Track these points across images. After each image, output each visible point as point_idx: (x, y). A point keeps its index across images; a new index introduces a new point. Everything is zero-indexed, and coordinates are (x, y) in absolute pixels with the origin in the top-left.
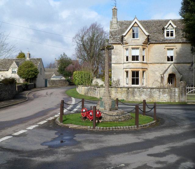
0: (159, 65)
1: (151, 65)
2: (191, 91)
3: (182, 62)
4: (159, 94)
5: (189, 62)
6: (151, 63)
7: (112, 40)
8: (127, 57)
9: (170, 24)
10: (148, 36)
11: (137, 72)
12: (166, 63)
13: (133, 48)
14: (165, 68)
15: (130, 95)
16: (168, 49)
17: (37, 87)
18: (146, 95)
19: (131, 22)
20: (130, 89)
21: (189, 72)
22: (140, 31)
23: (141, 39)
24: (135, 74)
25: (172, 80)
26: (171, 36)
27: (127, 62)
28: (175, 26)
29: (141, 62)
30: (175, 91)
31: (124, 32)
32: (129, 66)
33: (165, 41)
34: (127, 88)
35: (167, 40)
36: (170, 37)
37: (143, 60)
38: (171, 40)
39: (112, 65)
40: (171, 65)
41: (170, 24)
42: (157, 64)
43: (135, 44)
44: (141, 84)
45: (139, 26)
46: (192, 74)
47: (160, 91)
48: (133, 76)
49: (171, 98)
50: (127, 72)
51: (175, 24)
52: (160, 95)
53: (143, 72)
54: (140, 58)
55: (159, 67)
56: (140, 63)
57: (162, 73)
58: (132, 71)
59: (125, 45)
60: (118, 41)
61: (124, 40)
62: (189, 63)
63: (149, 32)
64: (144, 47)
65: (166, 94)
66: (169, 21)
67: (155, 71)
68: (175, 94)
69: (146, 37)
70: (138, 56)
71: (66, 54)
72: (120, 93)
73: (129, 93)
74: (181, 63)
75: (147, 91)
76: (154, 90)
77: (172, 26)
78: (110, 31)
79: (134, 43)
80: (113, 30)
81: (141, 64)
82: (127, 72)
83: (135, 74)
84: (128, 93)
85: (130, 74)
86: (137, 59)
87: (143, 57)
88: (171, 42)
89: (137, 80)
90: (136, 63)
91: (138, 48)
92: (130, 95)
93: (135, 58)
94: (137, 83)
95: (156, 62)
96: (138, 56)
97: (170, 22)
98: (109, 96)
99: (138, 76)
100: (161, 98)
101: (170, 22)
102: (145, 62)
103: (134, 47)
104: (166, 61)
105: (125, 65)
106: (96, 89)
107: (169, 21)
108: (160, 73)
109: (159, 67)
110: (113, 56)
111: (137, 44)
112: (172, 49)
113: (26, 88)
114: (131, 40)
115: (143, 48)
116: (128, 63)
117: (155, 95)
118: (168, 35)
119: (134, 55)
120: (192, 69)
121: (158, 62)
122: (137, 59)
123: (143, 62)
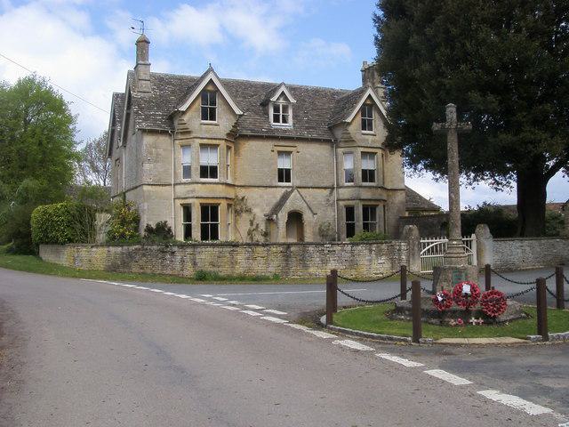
0: (260, 191)
2: (427, 248)
3: (310, 185)
6: (243, 184)
7: (144, 120)
9: (283, 93)
11: (215, 208)
12: (276, 187)
13: (203, 146)
14: (274, 197)
16: (280, 153)
18: (339, 260)
19: (198, 82)
20: (292, 249)
23: (223, 124)
24: (209, 212)
28: (292, 100)
29: (223, 181)
30: (399, 250)
32: (192, 191)
34: (284, 244)
40: (292, 191)
41: (283, 93)
47: (371, 251)
48: (204, 217)
51: (294, 96)
52: (370, 261)
56: (223, 184)
57: (268, 210)
59: (180, 137)
62: (325, 188)
66: (280, 86)
68: (400, 256)
70: (289, 170)
72: (262, 261)
75: (343, 250)
79: (207, 132)
81: (224, 187)
83: (209, 212)
89: (215, 228)
91: (215, 147)
92: (294, 264)
96: (190, 167)
97: (283, 89)
99: (215, 217)
100: (373, 266)
101: (283, 89)
103: (205, 141)
107: (280, 86)
108: (263, 211)
112: (288, 153)
113: (408, 221)
114: (199, 123)
115: (227, 146)
116: (190, 183)
118: (276, 119)
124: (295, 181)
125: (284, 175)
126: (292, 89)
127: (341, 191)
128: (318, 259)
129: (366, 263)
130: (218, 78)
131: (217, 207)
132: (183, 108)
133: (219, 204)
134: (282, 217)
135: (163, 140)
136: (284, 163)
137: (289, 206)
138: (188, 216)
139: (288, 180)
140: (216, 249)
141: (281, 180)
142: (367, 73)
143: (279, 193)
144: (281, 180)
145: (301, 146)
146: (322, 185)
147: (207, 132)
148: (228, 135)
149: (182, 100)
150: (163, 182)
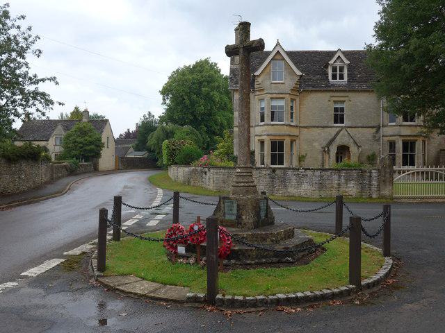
3: (360, 125)
5: (373, 124)
10: (301, 76)
11: (281, 143)
18: (311, 183)
20: (277, 172)
25: (341, 157)
28: (347, 62)
29: (287, 123)
31: (256, 70)
35: (333, 85)
36: (338, 80)
38: (340, 86)
40: (341, 130)
43: (277, 92)
45: (284, 59)
47: (340, 176)
48: (273, 149)
49: (362, 191)
53: (292, 142)
55: (319, 134)
57: (324, 144)
59: (258, 93)
61: (256, 83)
64: (294, 97)
69: (297, 79)
71: (153, 113)
74: (358, 127)
75: (314, 175)
77: (342, 61)
84: (273, 179)
85: (268, 146)
89: (281, 156)
95: (314, 124)
97: (339, 54)
99: (281, 149)
100: (342, 189)
103: (274, 96)
104: (332, 123)
106: (206, 173)
107: (336, 52)
109: (319, 134)
118: (334, 77)
123: (292, 124)
124: (347, 123)
127: (385, 129)
134: (334, 150)
137: (338, 141)
140: (226, 171)
141: (336, 122)
143: (333, 132)
144: (336, 122)
146: (370, 125)
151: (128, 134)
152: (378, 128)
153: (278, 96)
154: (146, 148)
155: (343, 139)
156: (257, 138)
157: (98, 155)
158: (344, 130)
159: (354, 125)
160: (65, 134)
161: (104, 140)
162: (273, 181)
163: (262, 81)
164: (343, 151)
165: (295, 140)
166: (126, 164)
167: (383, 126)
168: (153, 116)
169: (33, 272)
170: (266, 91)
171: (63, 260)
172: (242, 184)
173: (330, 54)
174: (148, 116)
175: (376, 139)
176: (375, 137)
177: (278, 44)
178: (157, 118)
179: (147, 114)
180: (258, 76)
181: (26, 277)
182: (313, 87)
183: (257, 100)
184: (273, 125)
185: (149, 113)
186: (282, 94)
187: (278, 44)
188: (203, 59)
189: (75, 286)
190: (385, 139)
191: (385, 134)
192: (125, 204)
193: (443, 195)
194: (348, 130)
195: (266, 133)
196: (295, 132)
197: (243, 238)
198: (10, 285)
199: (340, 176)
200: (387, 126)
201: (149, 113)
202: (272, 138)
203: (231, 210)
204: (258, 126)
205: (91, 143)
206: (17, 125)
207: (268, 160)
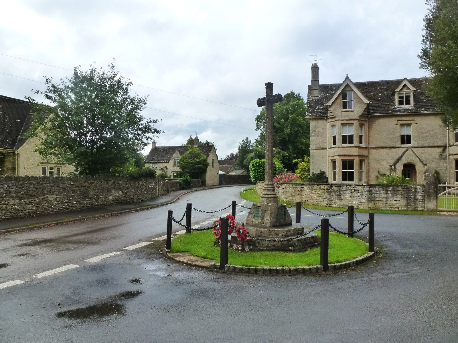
0: (387, 150)
1: (374, 150)
3: (426, 145)
4: (385, 196)
5: (440, 144)
7: (311, 113)
8: (334, 138)
9: (405, 85)
11: (351, 163)
12: (398, 148)
13: (343, 125)
14: (397, 154)
15: (334, 197)
16: (402, 125)
17: (207, 185)
19: (337, 86)
20: (334, 187)
21: (438, 161)
22: (355, 98)
23: (357, 110)
26: (406, 104)
27: (335, 146)
28: (413, 89)
30: (415, 191)
33: (397, 111)
35: (399, 110)
36: (405, 105)
37: (361, 142)
38: (406, 110)
39: (311, 151)
40: (407, 150)
41: (405, 85)
42: (384, 150)
43: (346, 118)
44: (357, 180)
46: (445, 165)
47: (387, 191)
48: (344, 166)
49: (408, 204)
50: (334, 162)
51: (414, 86)
52: (387, 198)
53: (361, 162)
54: (356, 140)
56: (356, 147)
57: (392, 162)
58: (341, 159)
59: (330, 120)
60: (320, 115)
61: (329, 112)
63: (369, 99)
65: (399, 196)
67: (381, 159)
68: (415, 196)
69: (364, 107)
71: (250, 139)
72: (317, 194)
73: (332, 194)
74: (425, 147)
76: (377, 188)
77: (408, 89)
78: (308, 101)
79: (346, 116)
80: (311, 98)
81: (357, 149)
82: (334, 162)
85: (339, 165)
86: (351, 142)
87: (361, 137)
88: (407, 113)
89: (351, 174)
90: (349, 148)
93: (347, 139)
94: (351, 179)
98: (273, 196)
99: (351, 167)
100: (389, 202)
102: (363, 145)
104: (399, 144)
105: (331, 152)
106: (279, 188)
108: (388, 163)
109: (387, 154)
110: (313, 137)
111: (351, 118)
112: (409, 125)
114: (340, 111)
115: (360, 124)
117: (378, 196)
118: (401, 103)
119: (403, 134)
120: (444, 157)
121: (385, 145)
122: (351, 142)
123: (361, 145)
124: (413, 143)
125: (406, 140)
126: (411, 81)
127: (451, 148)
128: (348, 195)
129: (383, 199)
130: (352, 82)
131: (353, 162)
132: (329, 103)
133: (354, 159)
134: (400, 167)
135: (321, 122)
136: (406, 132)
137: (404, 160)
138: (335, 167)
139: (409, 142)
140: (294, 186)
141: (403, 142)
142: (213, 133)
143: (401, 151)
144: (403, 142)
145: (419, 119)
146: (436, 145)
147: (346, 116)
148: (360, 117)
149: (328, 99)
150: (321, 147)
151: (232, 157)
152: (445, 148)
153: (348, 122)
154: (243, 169)
155: (409, 158)
156: (331, 158)
157: (204, 171)
158: (410, 150)
159: (421, 145)
160: (181, 157)
161: (209, 160)
162: (330, 195)
163: (334, 110)
164: (409, 170)
165: (364, 160)
166: (226, 181)
167: (450, 146)
168: (250, 141)
169: (130, 248)
170: (337, 119)
171: (150, 243)
172: (266, 196)
173: (397, 83)
174: (246, 141)
175: (442, 157)
176: (441, 155)
177: (347, 78)
178: (253, 141)
179: (245, 139)
180: (330, 106)
181: (127, 250)
182: (380, 113)
183: (330, 126)
184: (343, 147)
185: (247, 138)
186: (351, 120)
187: (347, 78)
188: (290, 92)
189: (151, 256)
190: (452, 157)
191: (451, 153)
192: (194, 209)
193: (456, 209)
194: (415, 150)
195: (337, 154)
196: (364, 153)
197: (261, 232)
198: (117, 253)
199: (387, 191)
200: (453, 145)
201: (247, 138)
202: (342, 158)
203: (258, 214)
204: (330, 148)
205: (199, 163)
206: (146, 151)
207: (339, 177)
